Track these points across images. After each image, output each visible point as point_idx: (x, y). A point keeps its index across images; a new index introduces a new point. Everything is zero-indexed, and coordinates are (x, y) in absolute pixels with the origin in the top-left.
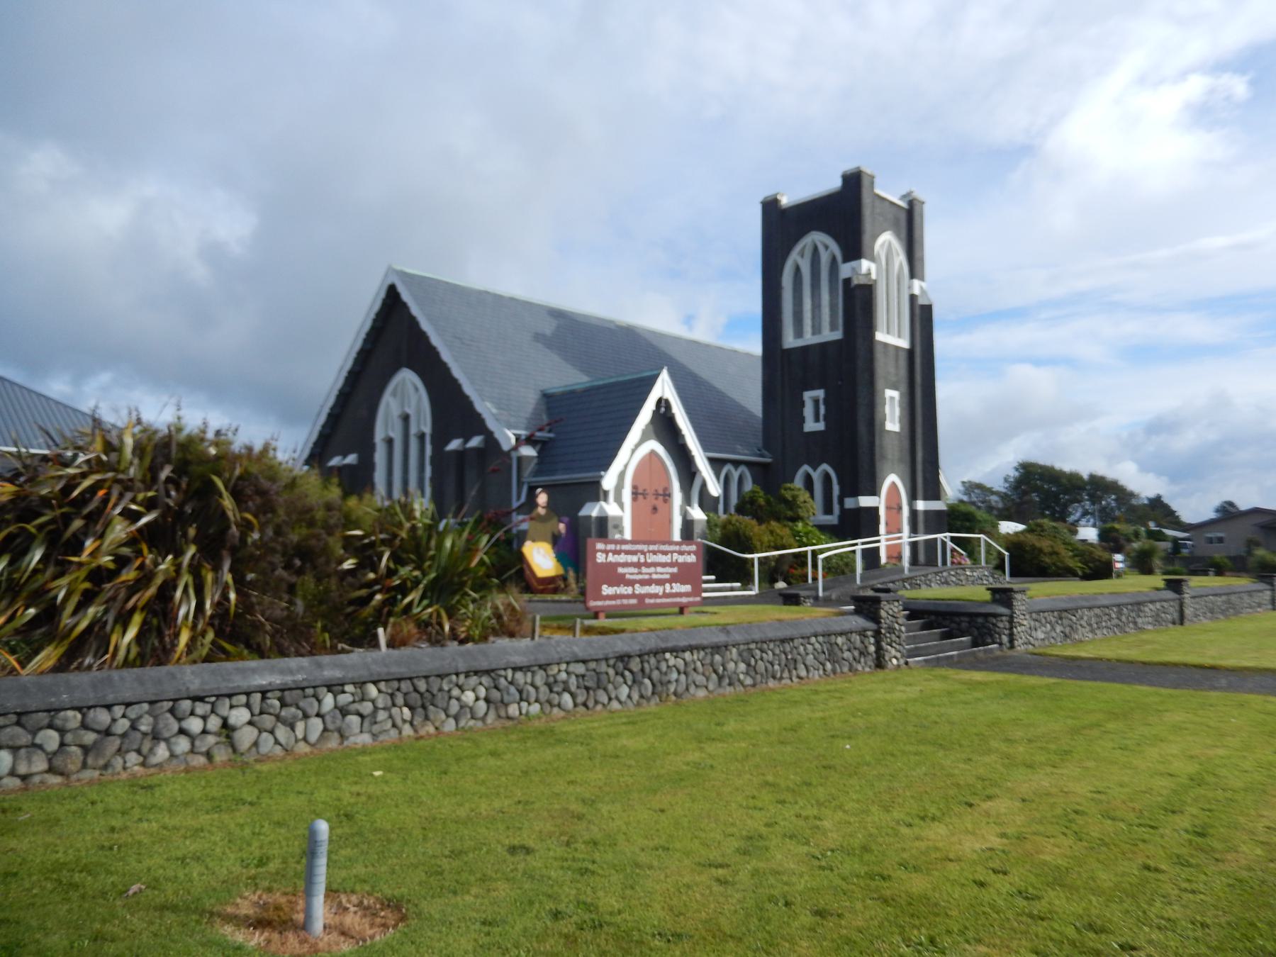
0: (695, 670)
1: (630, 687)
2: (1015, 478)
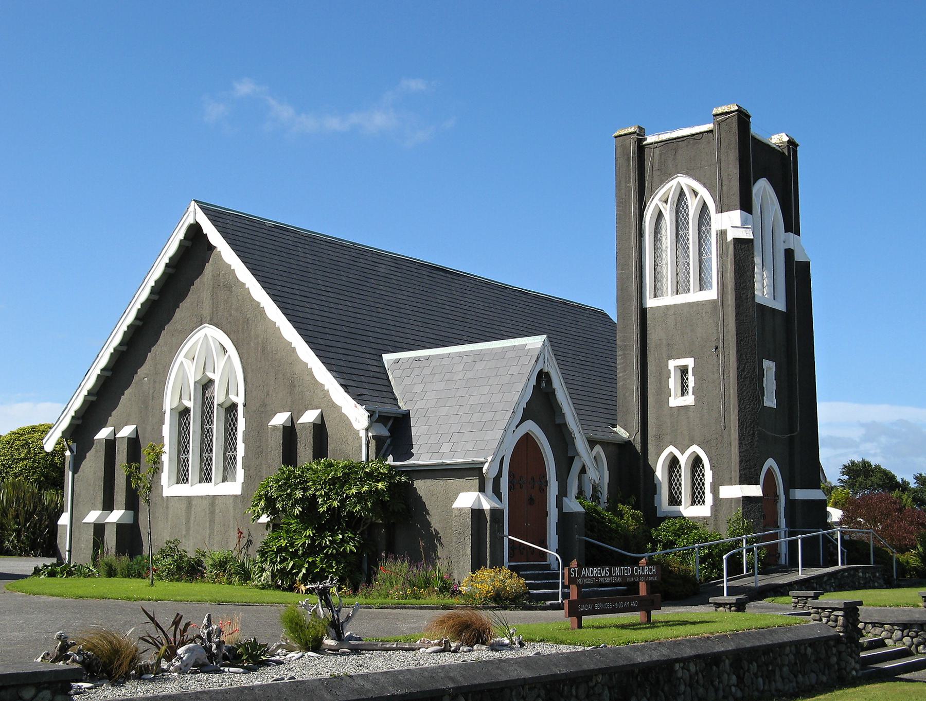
0: (697, 682)
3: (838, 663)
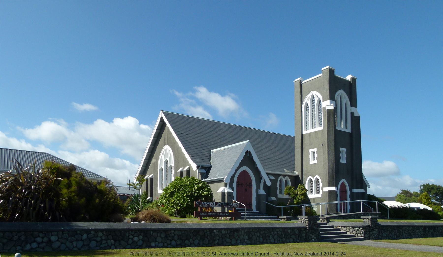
1: (199, 240)
3: (305, 236)
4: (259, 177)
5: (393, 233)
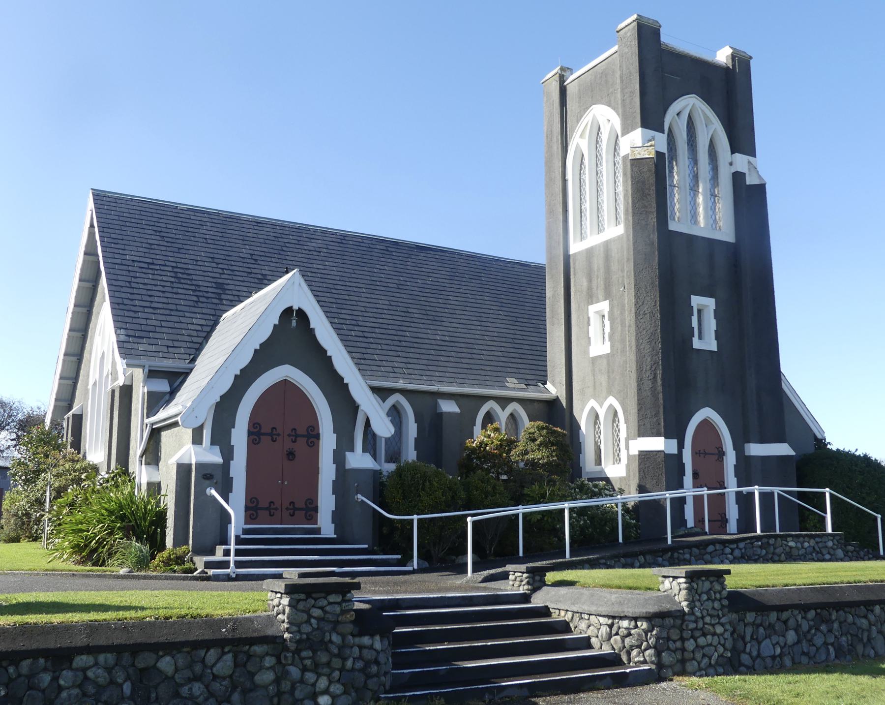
2: (407, 463)
3: (277, 681)
4: (345, 407)
5: (819, 640)
